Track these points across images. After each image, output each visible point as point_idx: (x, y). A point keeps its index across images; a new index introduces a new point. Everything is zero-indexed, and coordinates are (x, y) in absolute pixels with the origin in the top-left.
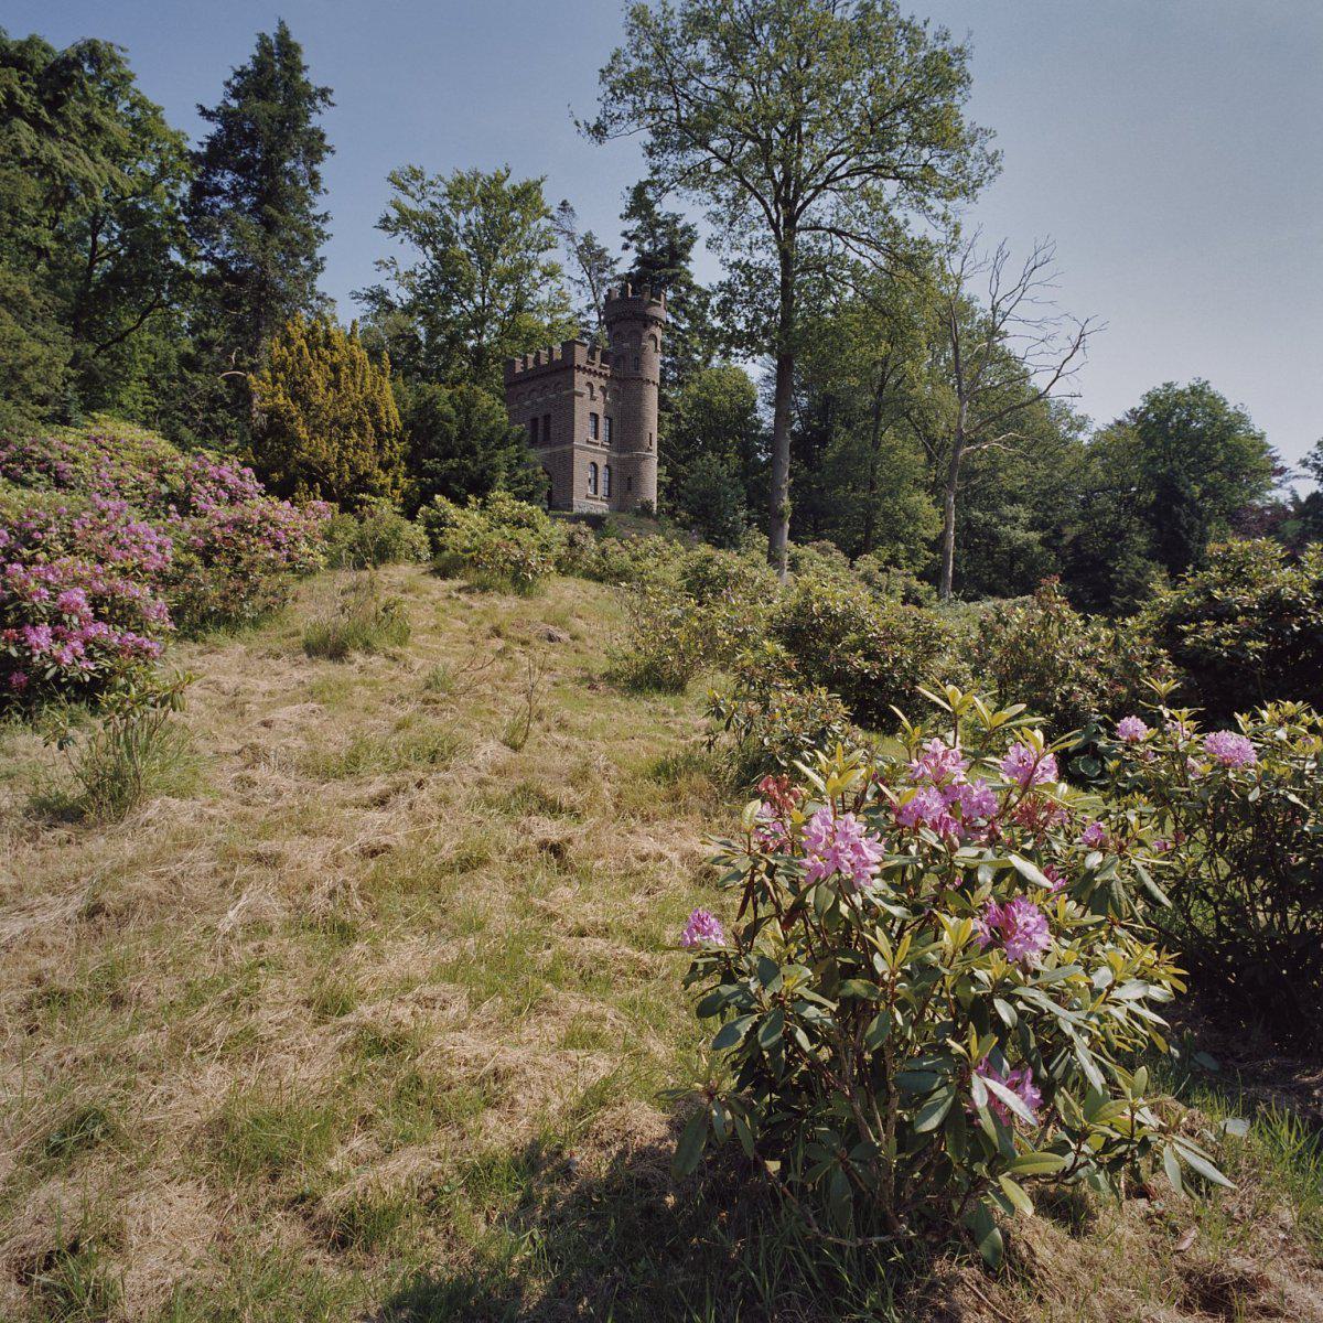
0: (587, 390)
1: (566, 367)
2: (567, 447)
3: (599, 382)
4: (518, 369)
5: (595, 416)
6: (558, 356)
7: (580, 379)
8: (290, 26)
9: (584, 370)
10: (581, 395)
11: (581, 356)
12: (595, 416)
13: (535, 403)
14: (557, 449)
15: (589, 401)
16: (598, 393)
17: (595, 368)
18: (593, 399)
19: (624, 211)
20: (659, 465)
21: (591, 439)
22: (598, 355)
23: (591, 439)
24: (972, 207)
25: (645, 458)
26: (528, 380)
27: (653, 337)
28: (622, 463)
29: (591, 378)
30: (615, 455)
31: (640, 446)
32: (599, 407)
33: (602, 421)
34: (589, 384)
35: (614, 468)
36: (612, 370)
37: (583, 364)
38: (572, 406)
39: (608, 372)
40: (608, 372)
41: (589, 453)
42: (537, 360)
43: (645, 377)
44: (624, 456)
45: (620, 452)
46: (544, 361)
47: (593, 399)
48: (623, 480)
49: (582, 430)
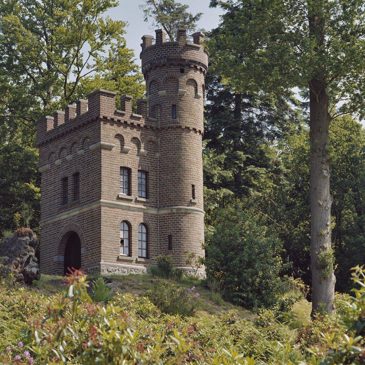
0: (116, 143)
1: (92, 121)
2: (94, 206)
3: (129, 134)
4: (50, 126)
5: (126, 171)
6: (85, 109)
7: (108, 133)
8: (202, 17)
9: (112, 122)
10: (109, 148)
11: (107, 107)
12: (126, 171)
13: (65, 161)
14: (85, 209)
15: (120, 153)
16: (130, 146)
17: (126, 118)
18: (124, 151)
19: (202, 15)
20: (208, 222)
21: (123, 195)
22: (128, 105)
23: (123, 195)
24: (199, 21)
25: (187, 213)
26: (59, 137)
27: (193, 82)
28: (161, 220)
29: (120, 130)
30: (153, 211)
31: (179, 198)
32: (132, 161)
33: (135, 175)
34: (119, 137)
35: (152, 226)
36: (147, 120)
37: (110, 115)
38: (99, 160)
39: (142, 122)
40: (142, 122)
41: (119, 215)
42: (78, 110)
43: (184, 124)
44: (163, 212)
45: (158, 208)
46: (61, 122)
47: (124, 151)
48: (163, 237)
49: (111, 185)
